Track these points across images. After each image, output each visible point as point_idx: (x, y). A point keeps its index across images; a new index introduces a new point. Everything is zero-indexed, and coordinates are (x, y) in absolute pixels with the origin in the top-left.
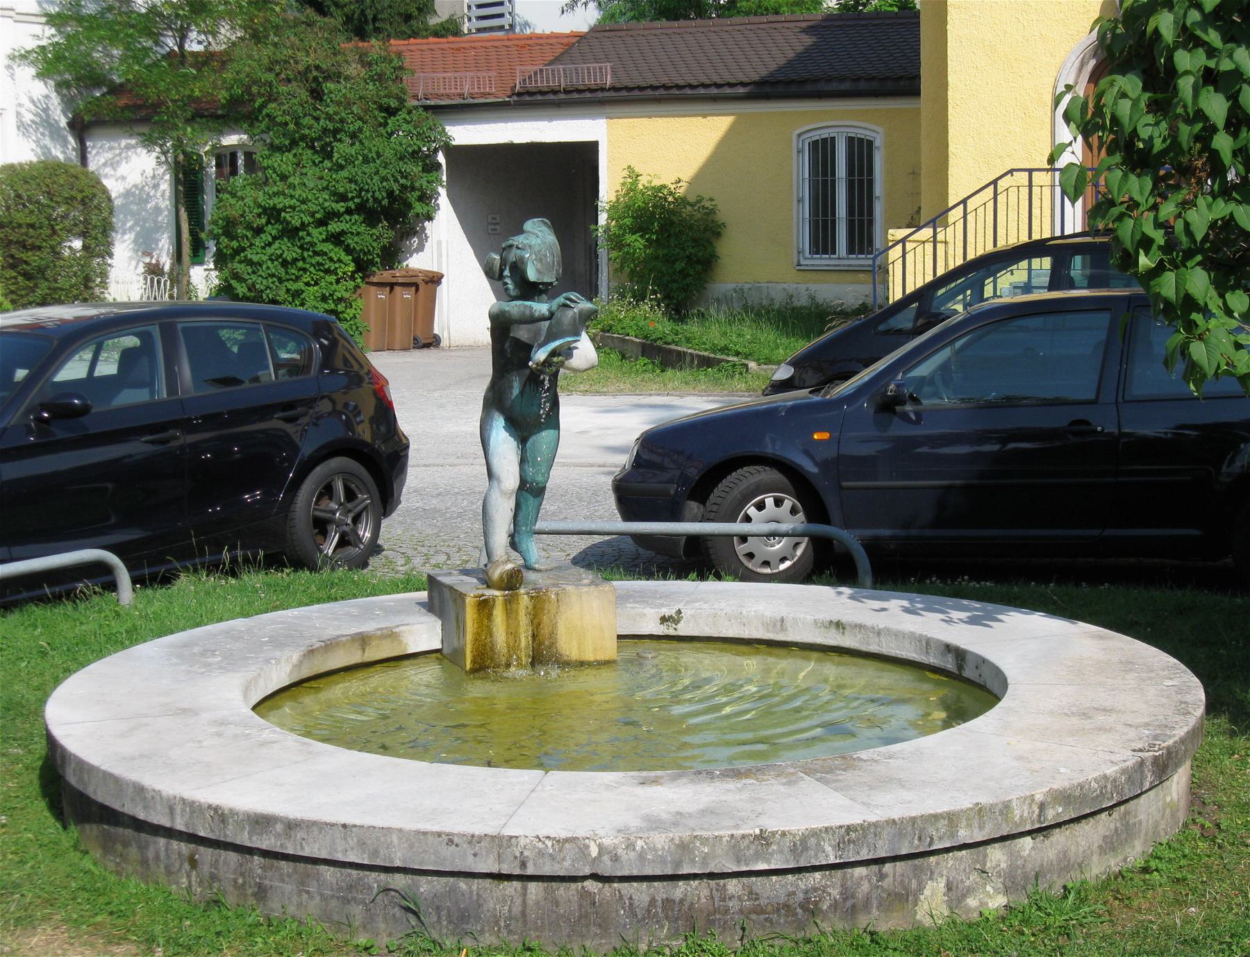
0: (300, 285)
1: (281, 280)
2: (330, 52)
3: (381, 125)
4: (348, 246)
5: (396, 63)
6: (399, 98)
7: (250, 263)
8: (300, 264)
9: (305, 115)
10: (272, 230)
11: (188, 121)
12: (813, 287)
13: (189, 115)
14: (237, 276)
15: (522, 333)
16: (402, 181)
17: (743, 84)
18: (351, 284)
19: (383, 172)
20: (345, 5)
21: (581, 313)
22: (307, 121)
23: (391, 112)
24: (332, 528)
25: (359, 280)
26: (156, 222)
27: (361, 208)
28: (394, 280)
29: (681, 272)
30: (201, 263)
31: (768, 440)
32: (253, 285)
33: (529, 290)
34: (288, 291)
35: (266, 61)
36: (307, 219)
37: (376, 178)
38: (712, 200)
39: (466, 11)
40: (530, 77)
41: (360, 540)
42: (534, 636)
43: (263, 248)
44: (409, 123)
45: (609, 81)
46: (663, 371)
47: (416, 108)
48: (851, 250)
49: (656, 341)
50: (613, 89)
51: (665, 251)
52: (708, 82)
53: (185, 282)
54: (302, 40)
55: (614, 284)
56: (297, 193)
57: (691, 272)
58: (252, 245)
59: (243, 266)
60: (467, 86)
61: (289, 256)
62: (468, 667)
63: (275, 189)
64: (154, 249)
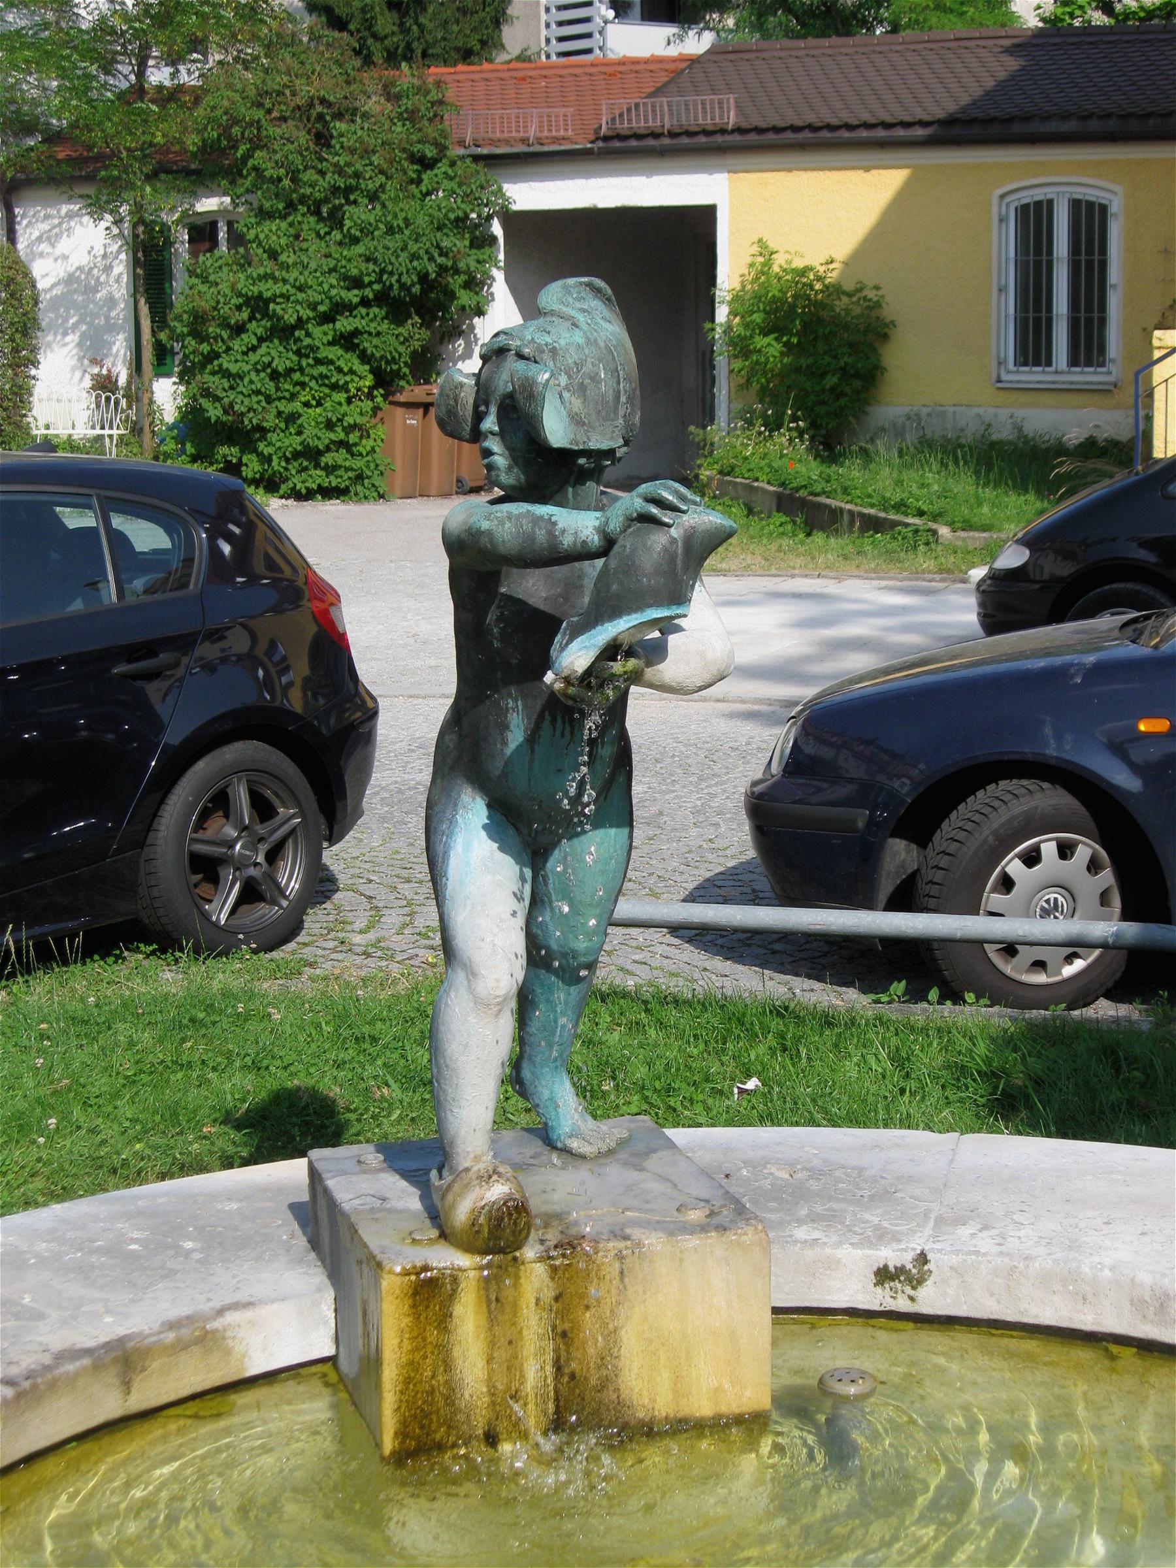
0: (296, 406)
1: (269, 399)
2: (341, 79)
3: (412, 181)
4: (364, 351)
5: (434, 95)
6: (436, 144)
7: (227, 374)
8: (297, 376)
9: (306, 168)
10: (257, 328)
11: (151, 177)
12: (1020, 413)
13: (147, 169)
14: (207, 393)
15: (533, 588)
16: (440, 260)
17: (922, 124)
18: (368, 405)
19: (413, 247)
20: (386, 37)
21: (689, 537)
22: (309, 176)
23: (427, 164)
24: (228, 874)
25: (379, 399)
26: (108, 318)
27: (382, 298)
28: (429, 399)
29: (832, 389)
30: (168, 375)
31: (1048, 730)
32: (231, 405)
33: (550, 472)
34: (279, 414)
35: (251, 92)
36: (306, 313)
37: (404, 255)
38: (877, 288)
39: (543, 44)
40: (621, 115)
41: (282, 892)
42: (558, 1367)
43: (245, 353)
44: (451, 179)
45: (732, 120)
46: (809, 535)
47: (462, 158)
48: (1074, 361)
49: (797, 489)
50: (739, 130)
51: (810, 361)
52: (873, 121)
53: (146, 401)
54: (302, 63)
55: (738, 406)
56: (293, 275)
57: (847, 389)
58: (228, 349)
59: (216, 378)
60: (532, 127)
61: (280, 365)
62: (388, 1444)
63: (261, 271)
64: (106, 356)
